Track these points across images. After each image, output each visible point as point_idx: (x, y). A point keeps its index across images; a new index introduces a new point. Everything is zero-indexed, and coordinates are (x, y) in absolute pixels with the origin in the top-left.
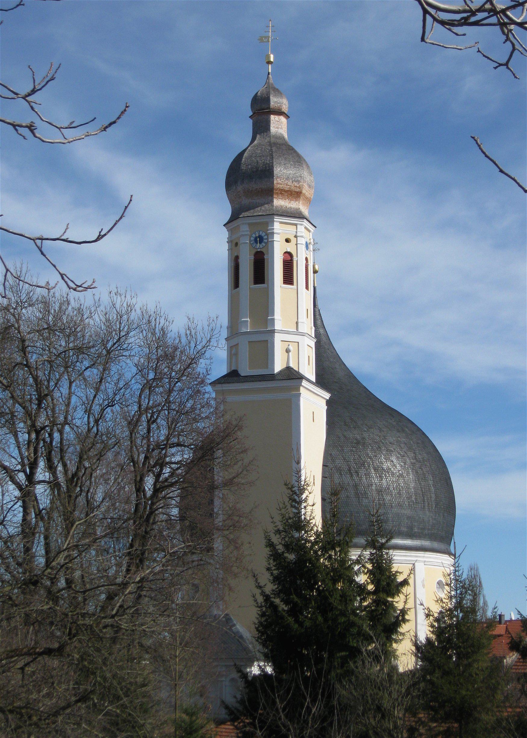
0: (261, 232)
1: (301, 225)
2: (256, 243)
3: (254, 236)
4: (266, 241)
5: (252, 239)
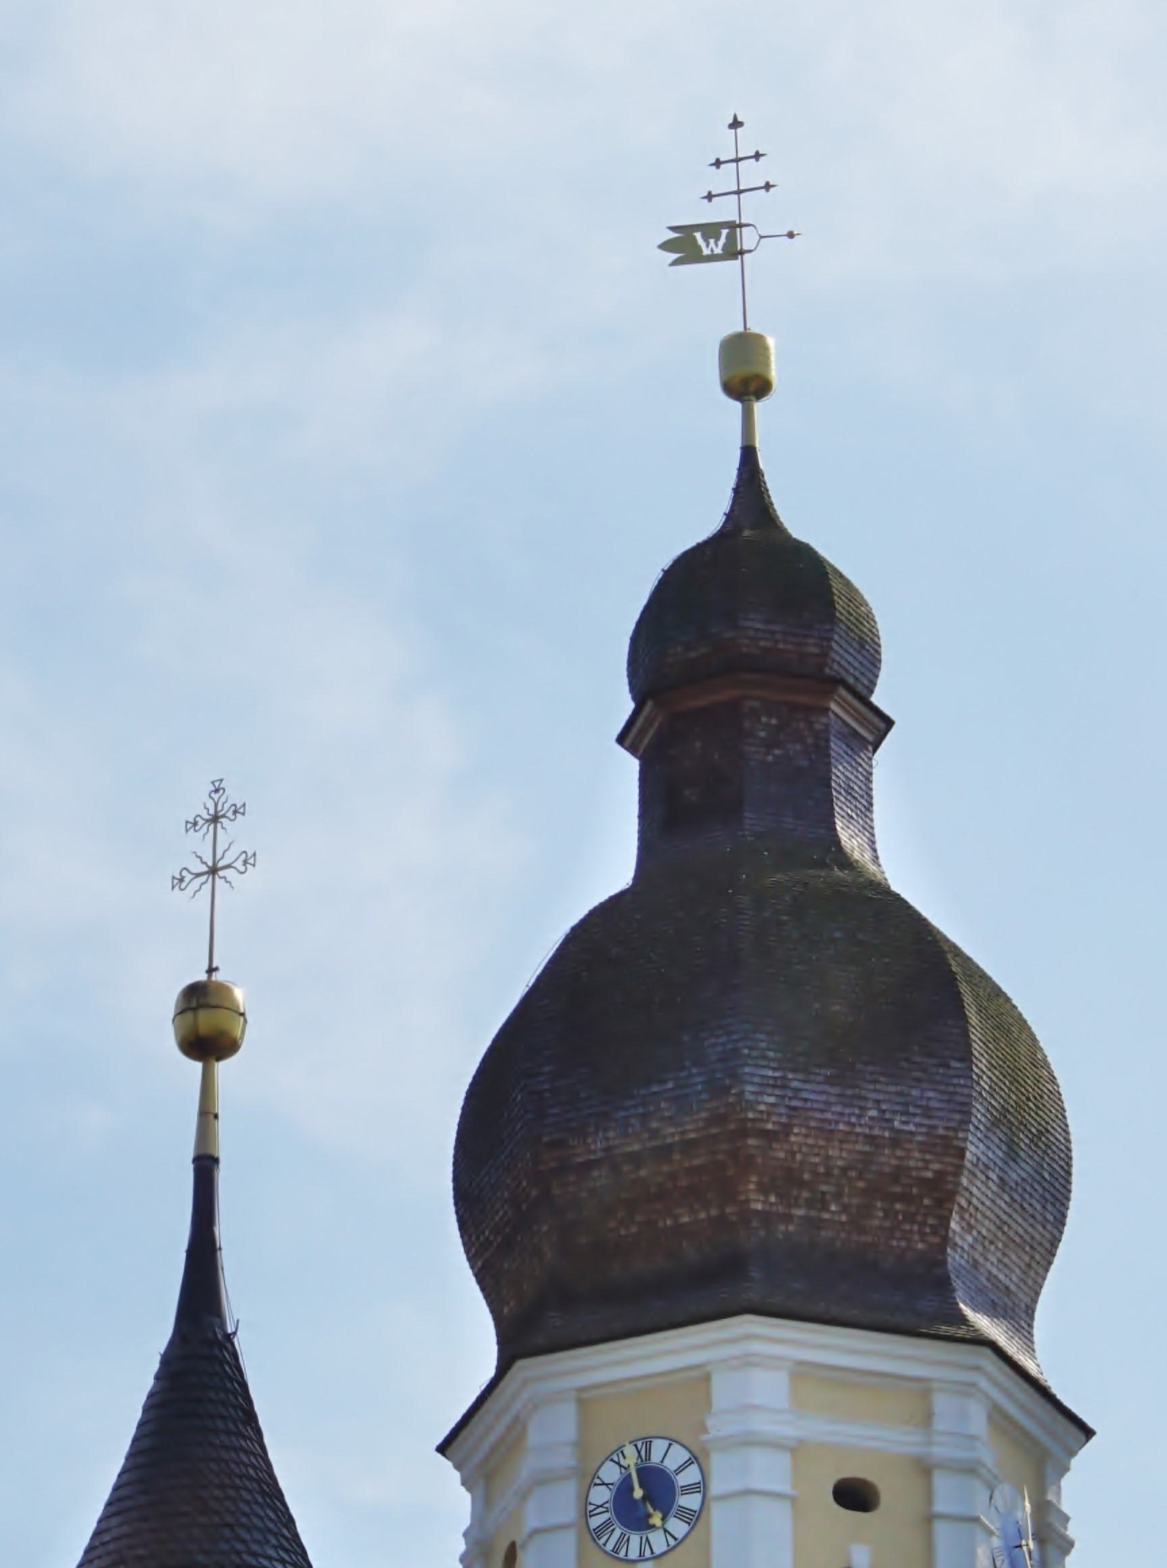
0: (658, 1447)
1: (748, 1362)
2: (642, 1524)
3: (611, 1473)
4: (691, 1501)
5: (601, 1495)
